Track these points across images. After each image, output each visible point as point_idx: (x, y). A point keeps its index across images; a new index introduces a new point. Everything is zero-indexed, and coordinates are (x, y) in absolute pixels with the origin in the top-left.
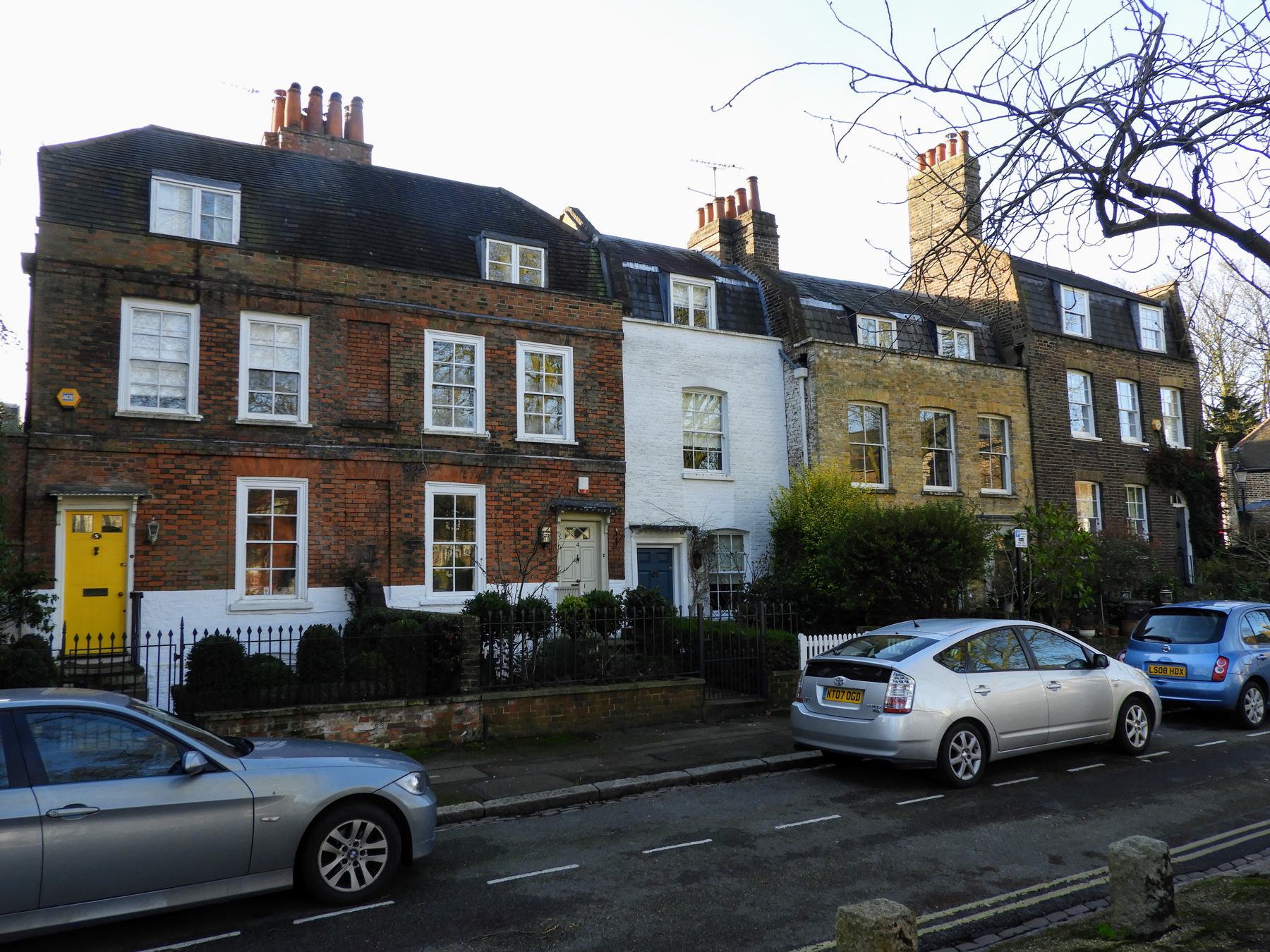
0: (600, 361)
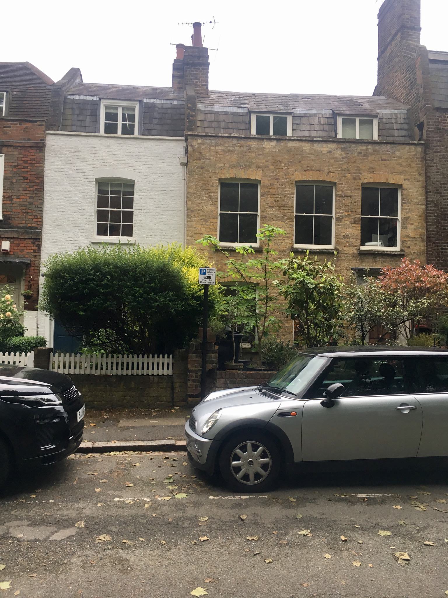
0: (25, 162)
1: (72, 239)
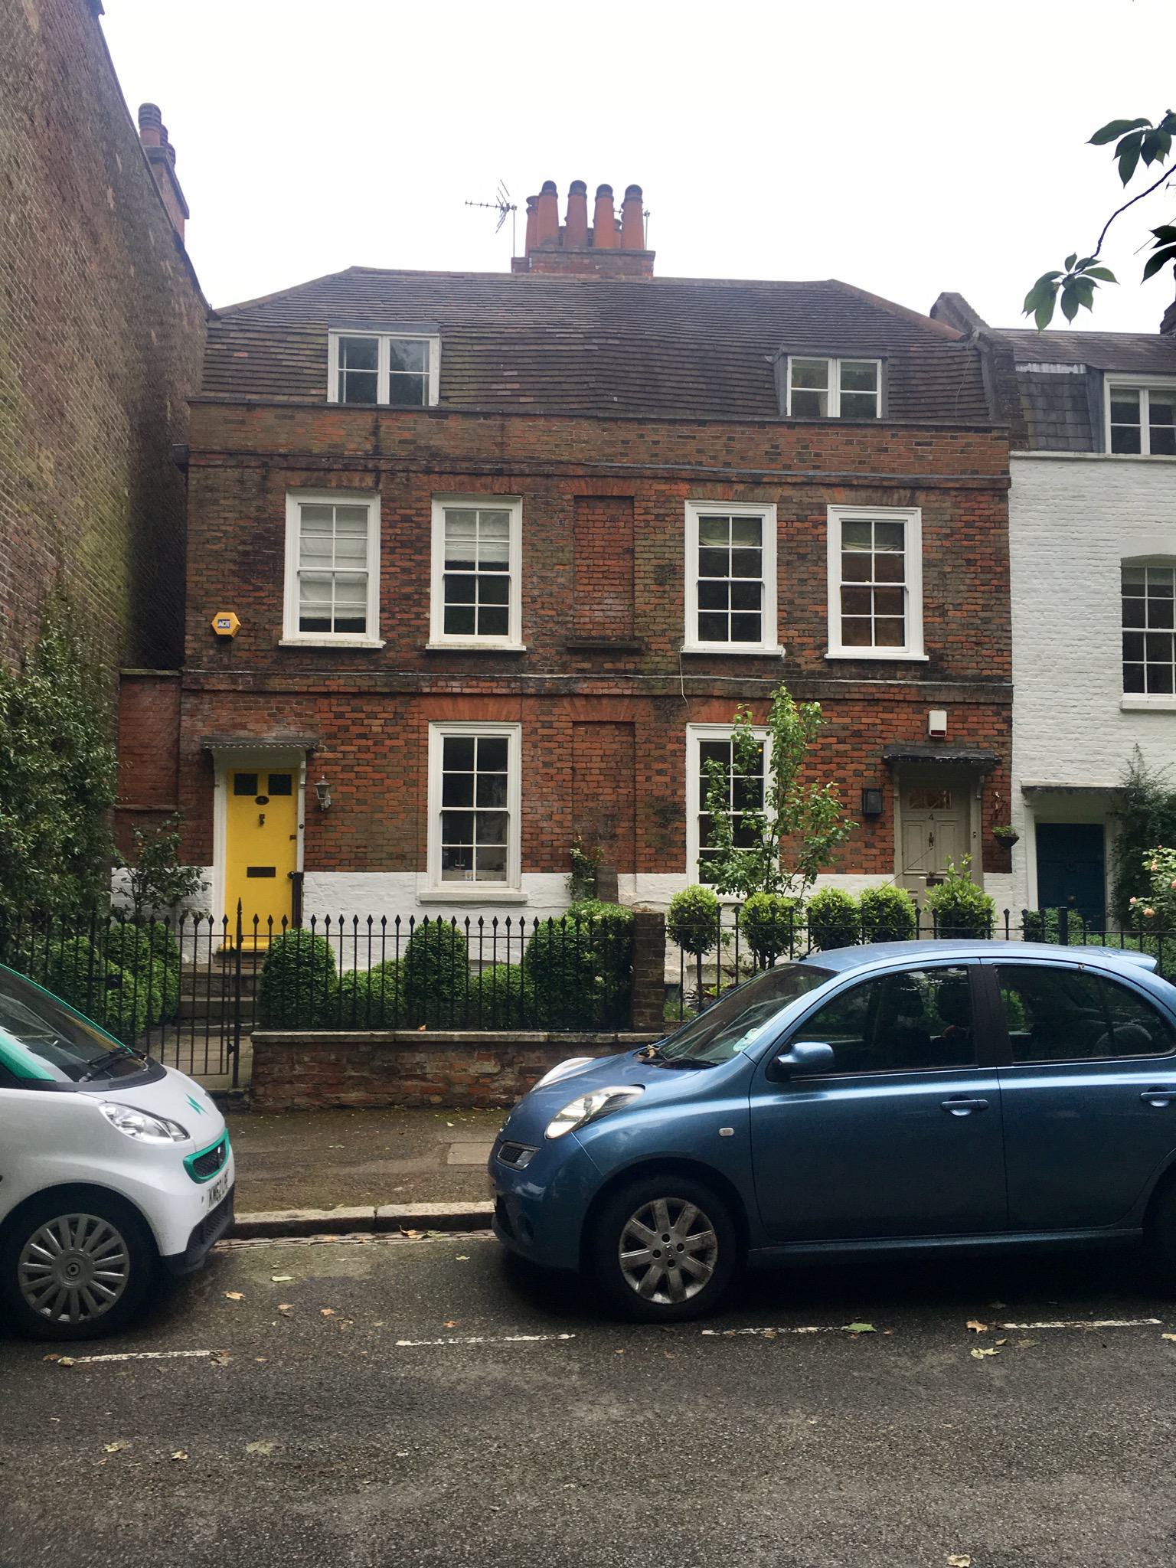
0: (969, 525)
1: (1076, 703)
